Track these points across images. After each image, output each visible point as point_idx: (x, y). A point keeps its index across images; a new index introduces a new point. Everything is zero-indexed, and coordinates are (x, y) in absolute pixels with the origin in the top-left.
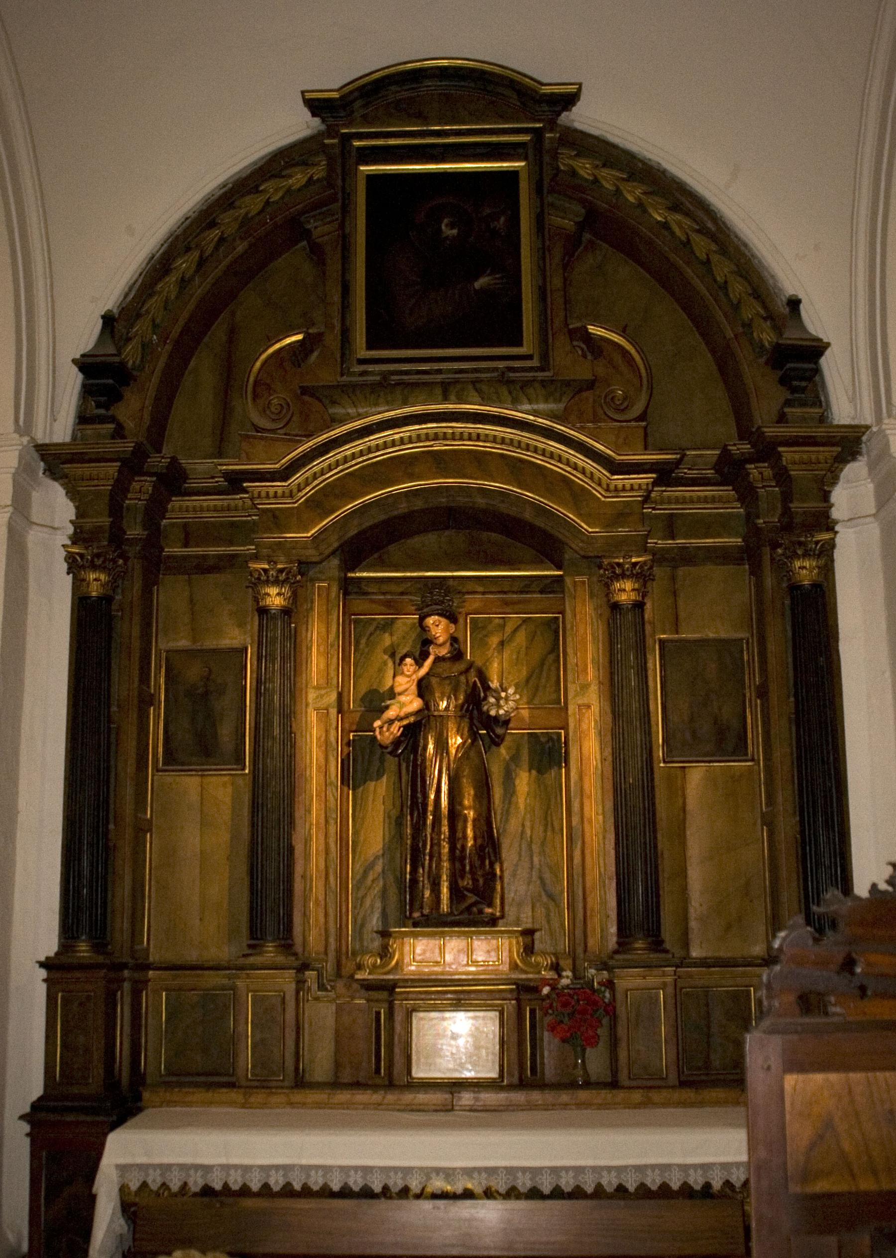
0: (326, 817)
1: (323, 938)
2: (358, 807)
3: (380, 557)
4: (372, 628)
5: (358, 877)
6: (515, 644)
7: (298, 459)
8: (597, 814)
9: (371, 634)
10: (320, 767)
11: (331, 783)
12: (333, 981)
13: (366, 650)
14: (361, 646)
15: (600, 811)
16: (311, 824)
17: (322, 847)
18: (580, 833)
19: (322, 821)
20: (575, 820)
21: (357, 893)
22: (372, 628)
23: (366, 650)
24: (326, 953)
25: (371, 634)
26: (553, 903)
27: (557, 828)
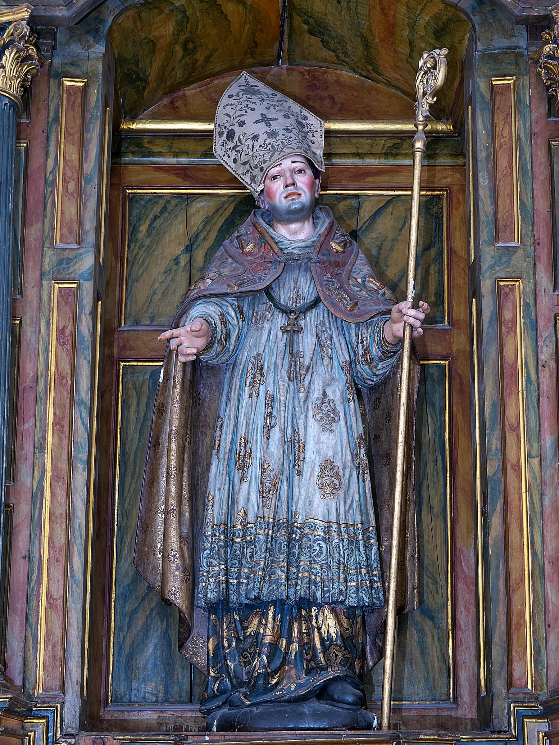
0: (69, 459)
1: (59, 663)
2: (129, 476)
3: (172, 102)
4: (157, 209)
5: (127, 581)
6: (374, 235)
7: (101, 365)
8: (530, 456)
9: (155, 218)
10: (63, 377)
11: (81, 402)
12: (71, 735)
13: (148, 242)
14: (140, 236)
15: (535, 452)
16: (44, 470)
17: (61, 510)
18: (501, 487)
19: (64, 464)
20: (493, 467)
21: (124, 607)
22: (157, 209)
23: (148, 242)
24: (62, 688)
25: (155, 218)
26: (430, 623)
27: (437, 508)
